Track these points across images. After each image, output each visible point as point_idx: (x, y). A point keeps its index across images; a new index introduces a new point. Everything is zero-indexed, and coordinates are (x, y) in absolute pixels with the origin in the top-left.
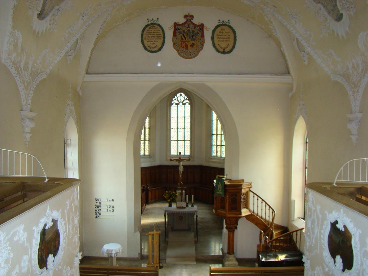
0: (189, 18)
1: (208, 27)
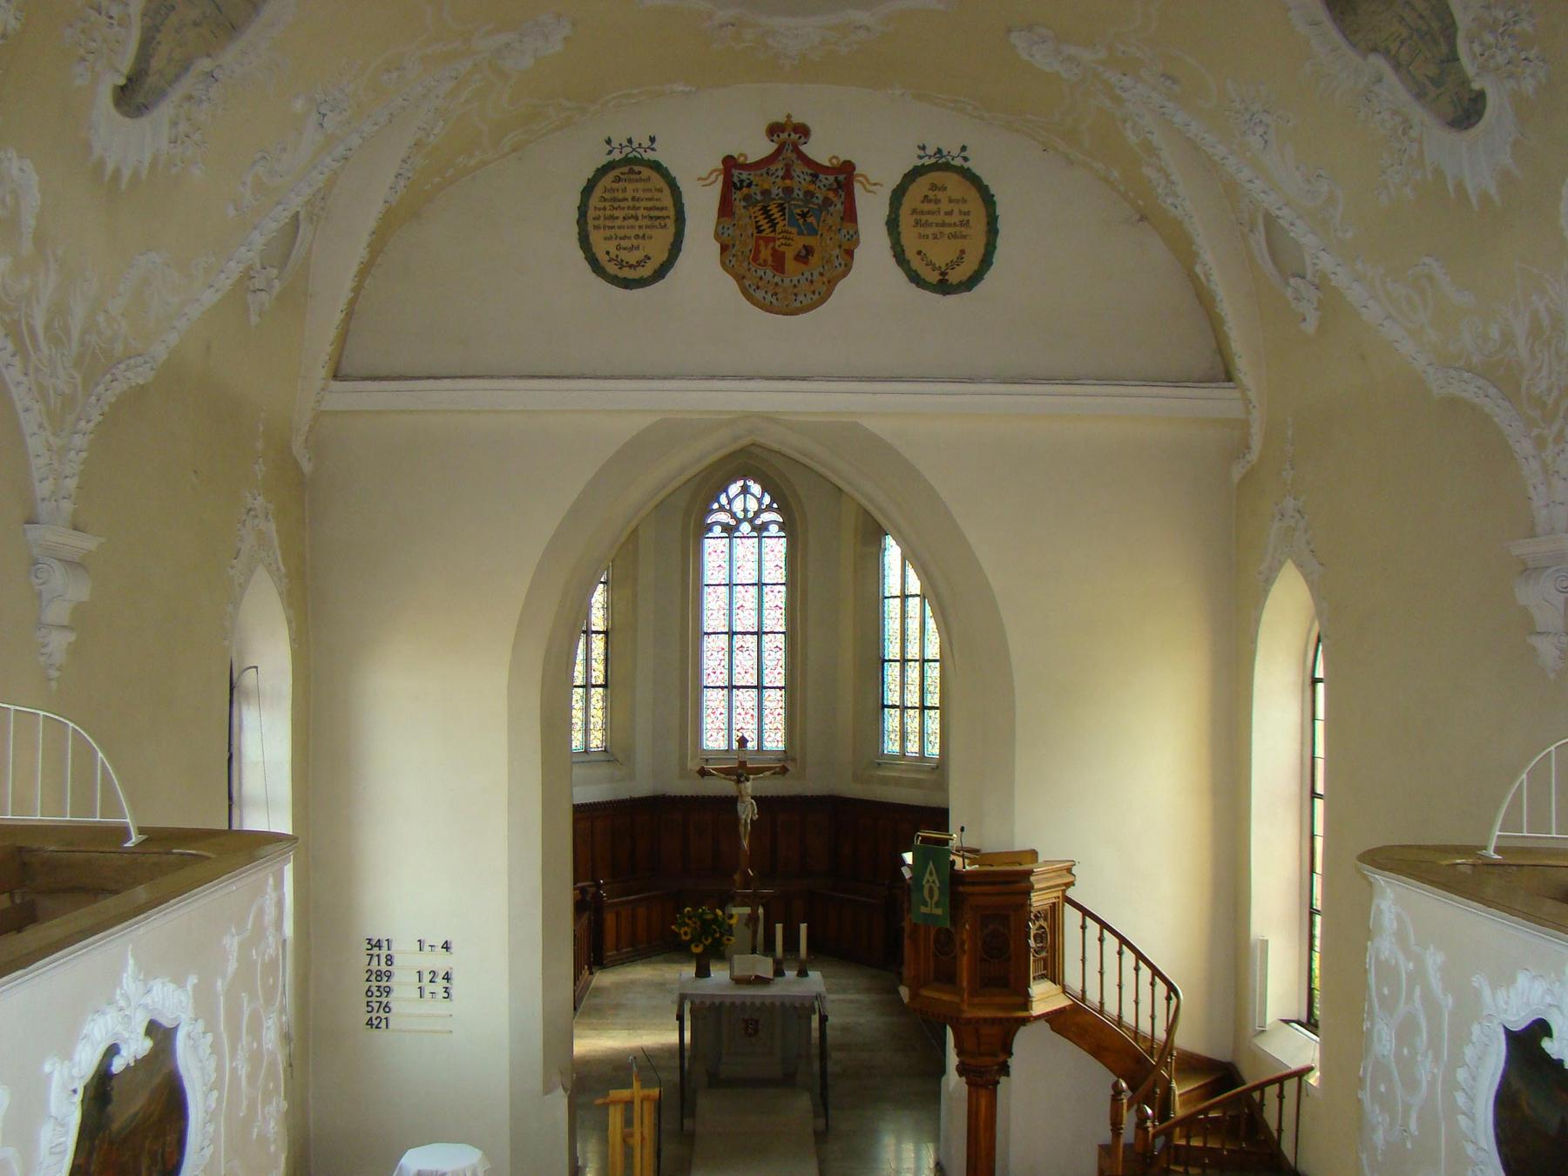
0: (790, 134)
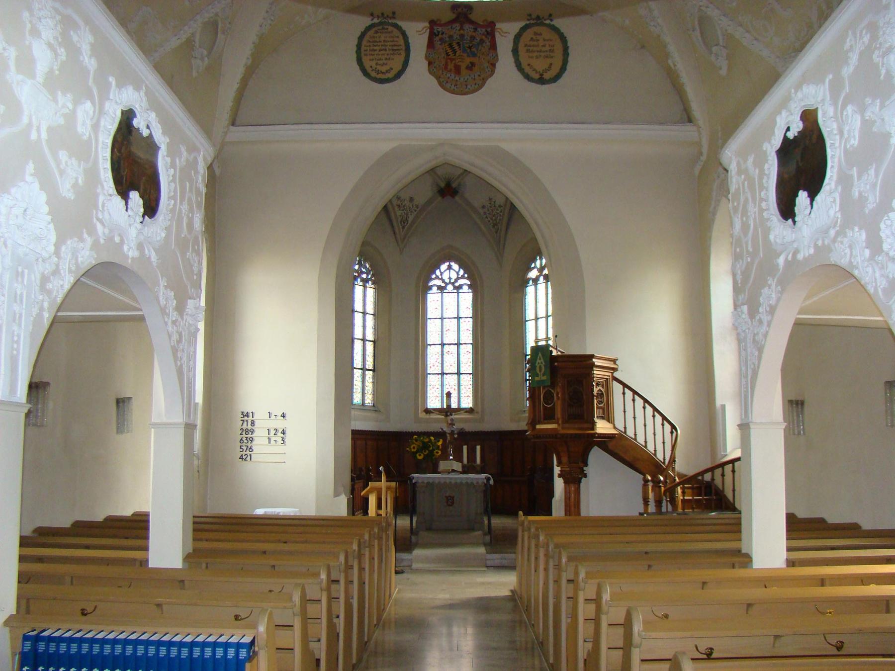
1: (504, 30)
